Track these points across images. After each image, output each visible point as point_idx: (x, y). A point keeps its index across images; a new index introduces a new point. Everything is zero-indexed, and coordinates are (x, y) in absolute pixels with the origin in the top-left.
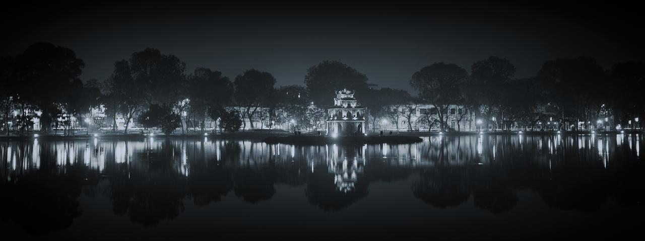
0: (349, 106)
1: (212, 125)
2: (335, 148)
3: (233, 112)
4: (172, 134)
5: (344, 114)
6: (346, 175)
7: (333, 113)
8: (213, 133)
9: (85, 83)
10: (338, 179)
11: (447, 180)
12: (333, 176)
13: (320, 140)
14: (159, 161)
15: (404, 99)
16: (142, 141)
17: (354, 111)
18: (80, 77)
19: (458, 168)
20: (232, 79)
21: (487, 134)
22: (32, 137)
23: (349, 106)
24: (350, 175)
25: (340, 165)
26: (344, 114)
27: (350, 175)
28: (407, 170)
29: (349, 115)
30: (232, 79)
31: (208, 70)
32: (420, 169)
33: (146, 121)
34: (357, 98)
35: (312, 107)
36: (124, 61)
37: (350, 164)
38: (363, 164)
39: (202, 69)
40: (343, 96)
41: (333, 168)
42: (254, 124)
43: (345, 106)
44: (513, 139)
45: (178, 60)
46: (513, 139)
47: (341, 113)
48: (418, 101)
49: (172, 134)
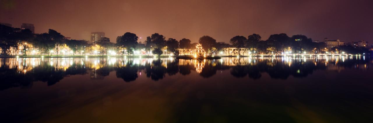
0: (200, 48)
1: (172, 54)
2: (196, 61)
3: (177, 50)
4: (161, 56)
5: (199, 51)
6: (199, 68)
7: (195, 50)
8: (277, 50)
9: (138, 42)
10: (197, 69)
11: (240, 70)
12: (196, 68)
13: (190, 58)
14: (158, 63)
15: (227, 46)
16: (153, 58)
17: (201, 50)
18: (137, 41)
19: (243, 67)
20: (179, 41)
21: (253, 56)
22: (261, 50)
23: (200, 48)
24: (200, 68)
25: (197, 65)
26: (199, 51)
27: (200, 68)
28: (228, 67)
29: (200, 51)
30: (179, 41)
31: (172, 39)
32: (232, 67)
33: (154, 52)
34: (203, 46)
35: (300, 45)
36: (149, 37)
37: (200, 65)
38: (272, 62)
39: (170, 38)
40: (198, 46)
41: (195, 66)
42: (185, 53)
43: (199, 48)
44: (260, 58)
45: (163, 36)
46: (260, 58)
47: (197, 50)
48: (232, 46)
49: (161, 56)
